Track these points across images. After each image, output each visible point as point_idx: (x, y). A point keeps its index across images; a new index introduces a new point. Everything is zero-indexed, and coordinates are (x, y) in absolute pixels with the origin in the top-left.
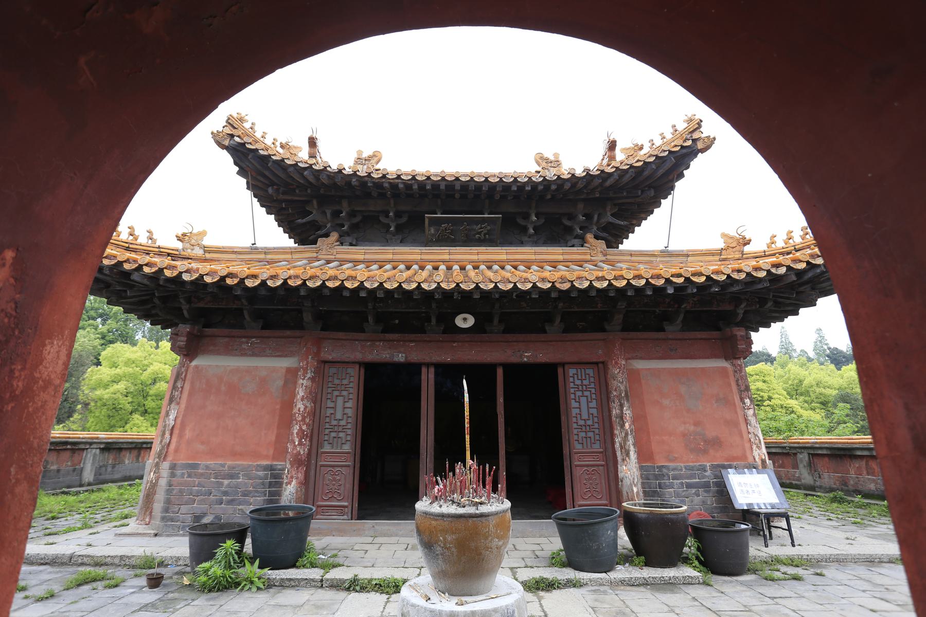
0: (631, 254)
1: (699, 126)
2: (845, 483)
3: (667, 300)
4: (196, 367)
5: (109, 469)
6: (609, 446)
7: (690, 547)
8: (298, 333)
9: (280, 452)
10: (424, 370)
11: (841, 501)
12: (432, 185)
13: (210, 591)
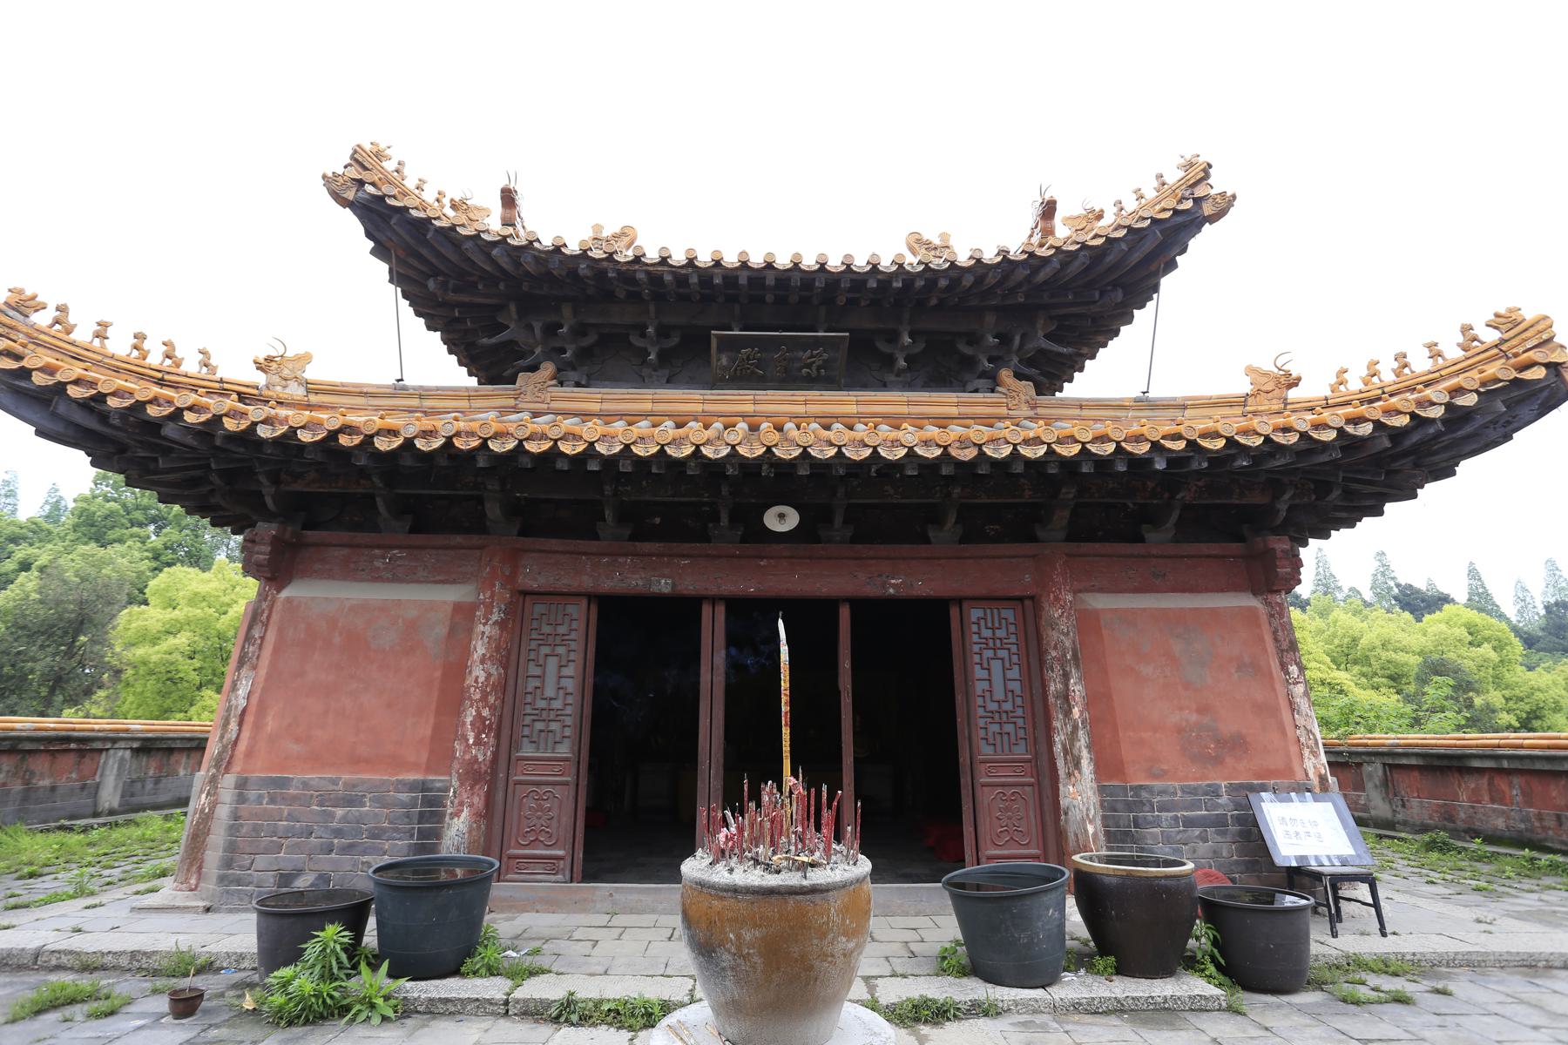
0: (1081, 404)
1: (1207, 176)
2: (1449, 816)
3: (1150, 485)
4: (289, 600)
5: (149, 786)
6: (1043, 748)
7: (1200, 939)
8: (475, 540)
9: (440, 755)
10: (706, 610)
11: (1444, 848)
12: (725, 278)
13: (290, 1023)
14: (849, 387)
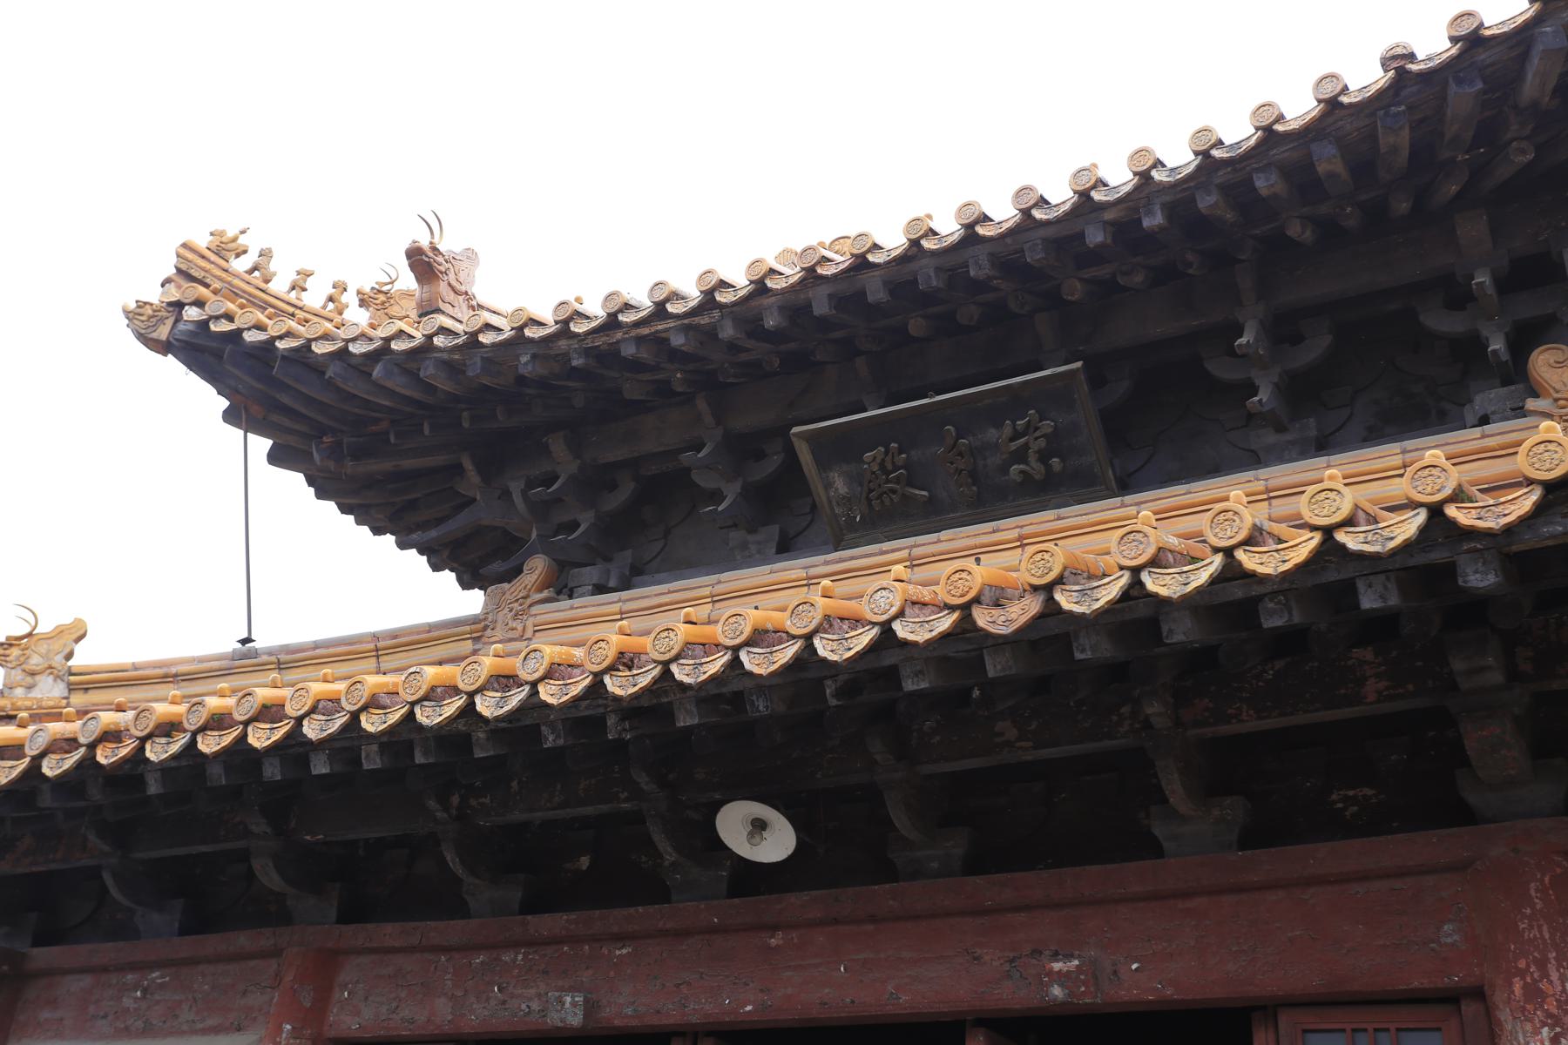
14: (1126, 485)
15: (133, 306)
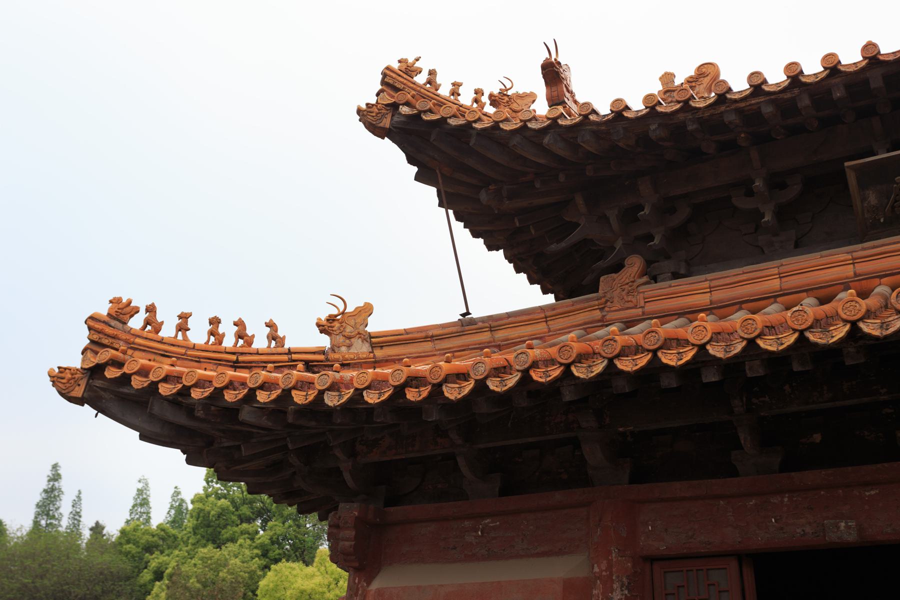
4: (380, 593)
15: (364, 107)
